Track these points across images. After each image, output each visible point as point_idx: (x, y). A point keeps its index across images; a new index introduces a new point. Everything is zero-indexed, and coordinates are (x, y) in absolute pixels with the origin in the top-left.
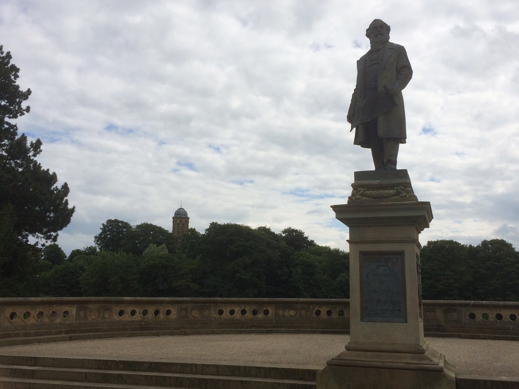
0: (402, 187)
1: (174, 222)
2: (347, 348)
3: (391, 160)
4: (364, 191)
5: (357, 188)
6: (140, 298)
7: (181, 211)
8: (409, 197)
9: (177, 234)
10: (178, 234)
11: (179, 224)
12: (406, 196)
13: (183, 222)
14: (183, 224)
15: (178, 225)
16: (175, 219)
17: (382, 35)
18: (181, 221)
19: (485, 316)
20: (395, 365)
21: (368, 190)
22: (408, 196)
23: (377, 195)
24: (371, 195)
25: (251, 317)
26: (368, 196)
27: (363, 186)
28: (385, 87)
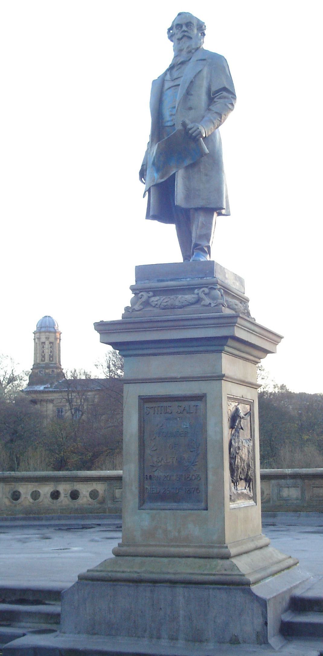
0: (206, 290)
1: (36, 340)
2: (117, 554)
3: (199, 245)
4: (149, 297)
5: (139, 292)
6: (52, 472)
7: (47, 321)
8: (215, 306)
9: (42, 360)
10: (42, 361)
11: (44, 343)
12: (210, 304)
13: (52, 340)
14: (50, 343)
15: (43, 345)
16: (38, 334)
17: (190, 38)
18: (47, 338)
19: (35, 495)
20: (119, 575)
21: (154, 296)
22: (213, 305)
23: (166, 304)
24: (157, 304)
25: (68, 502)
26: (154, 306)
27: (147, 290)
28: (184, 125)
